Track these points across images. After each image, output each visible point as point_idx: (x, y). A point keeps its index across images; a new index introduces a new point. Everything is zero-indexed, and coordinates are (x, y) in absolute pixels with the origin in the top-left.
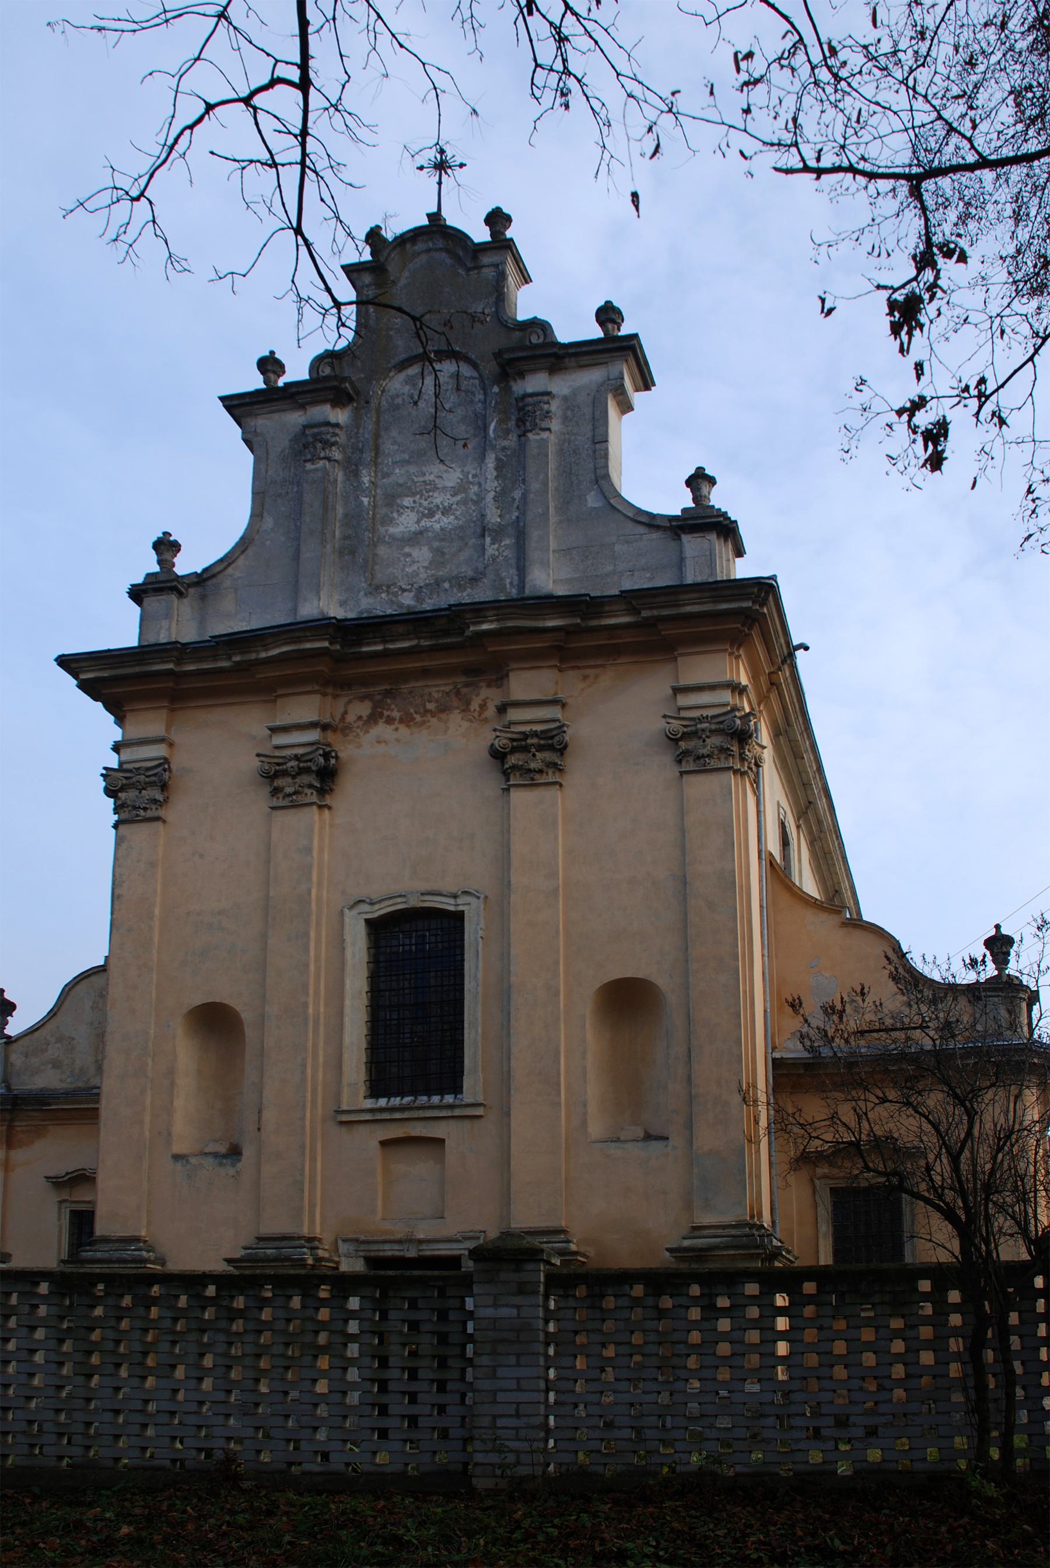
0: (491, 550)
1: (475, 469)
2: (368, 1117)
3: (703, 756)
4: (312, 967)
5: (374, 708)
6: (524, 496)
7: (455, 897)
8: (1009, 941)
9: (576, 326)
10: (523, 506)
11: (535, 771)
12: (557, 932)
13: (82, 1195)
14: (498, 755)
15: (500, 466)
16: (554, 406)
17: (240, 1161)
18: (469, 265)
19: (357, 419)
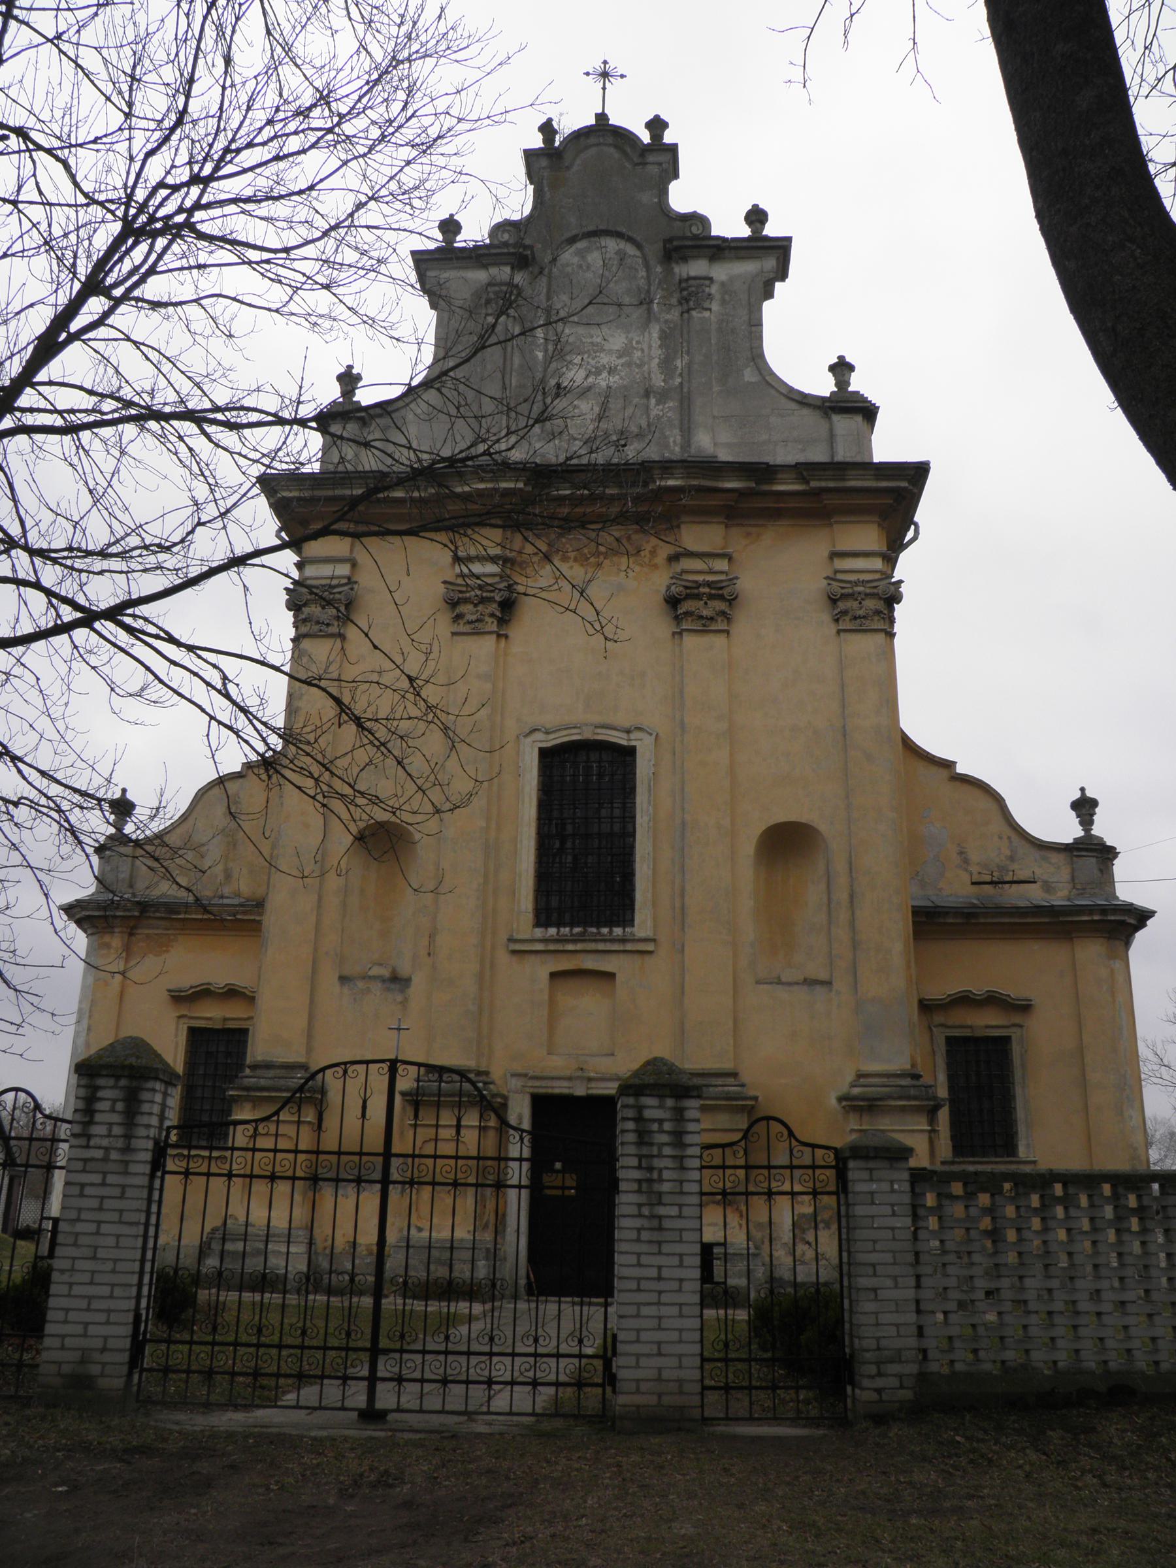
0: (655, 411)
2: (540, 947)
3: (860, 617)
6: (689, 365)
7: (628, 732)
8: (1094, 803)
9: (729, 225)
14: (673, 602)
15: (664, 336)
16: (714, 289)
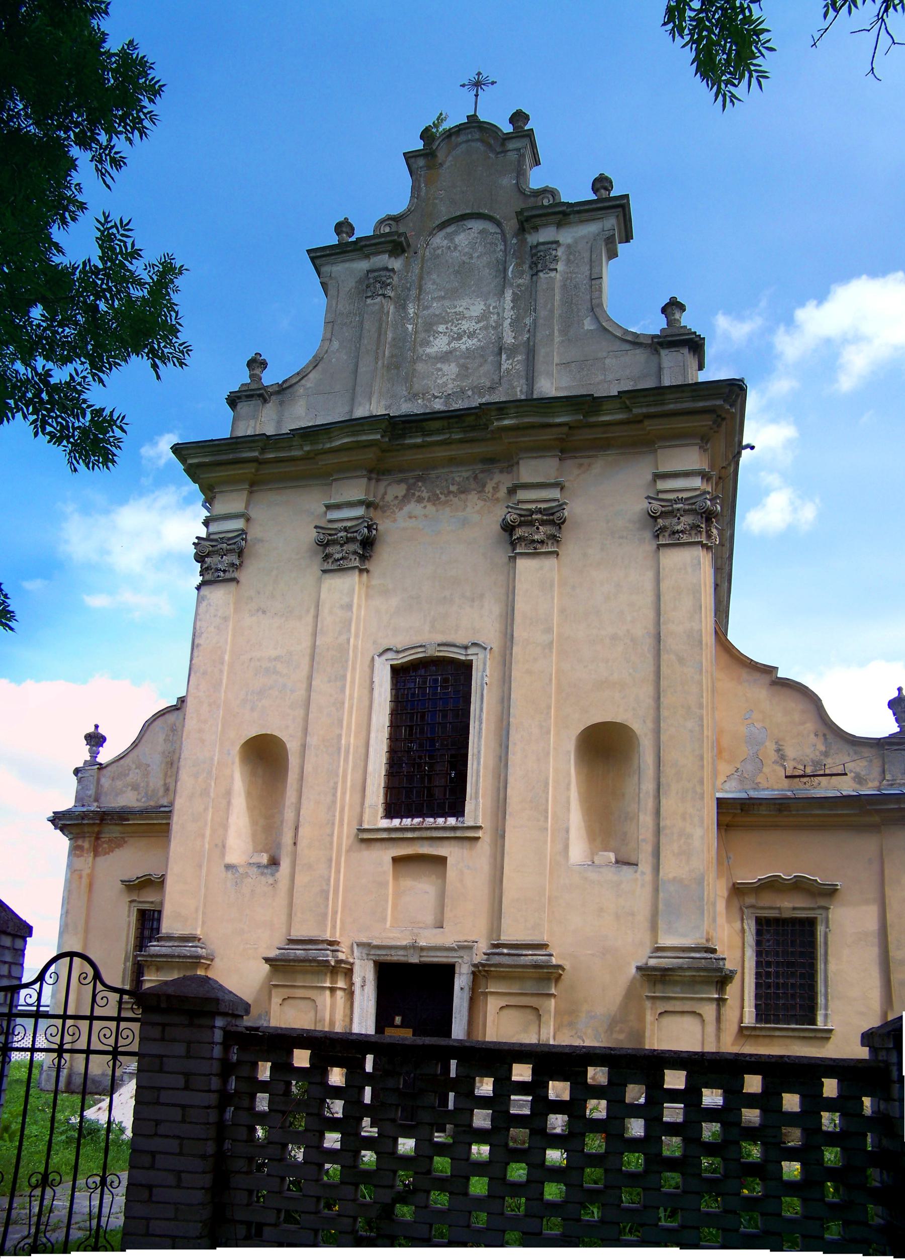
1: (495, 302)
2: (385, 835)
3: (678, 532)
4: (346, 705)
5: (408, 490)
6: (535, 321)
7: (466, 648)
9: (576, 190)
10: (533, 330)
11: (538, 542)
12: (551, 680)
13: (149, 897)
14: (508, 528)
16: (560, 252)
17: (278, 871)
18: (498, 150)
19: (407, 265)
